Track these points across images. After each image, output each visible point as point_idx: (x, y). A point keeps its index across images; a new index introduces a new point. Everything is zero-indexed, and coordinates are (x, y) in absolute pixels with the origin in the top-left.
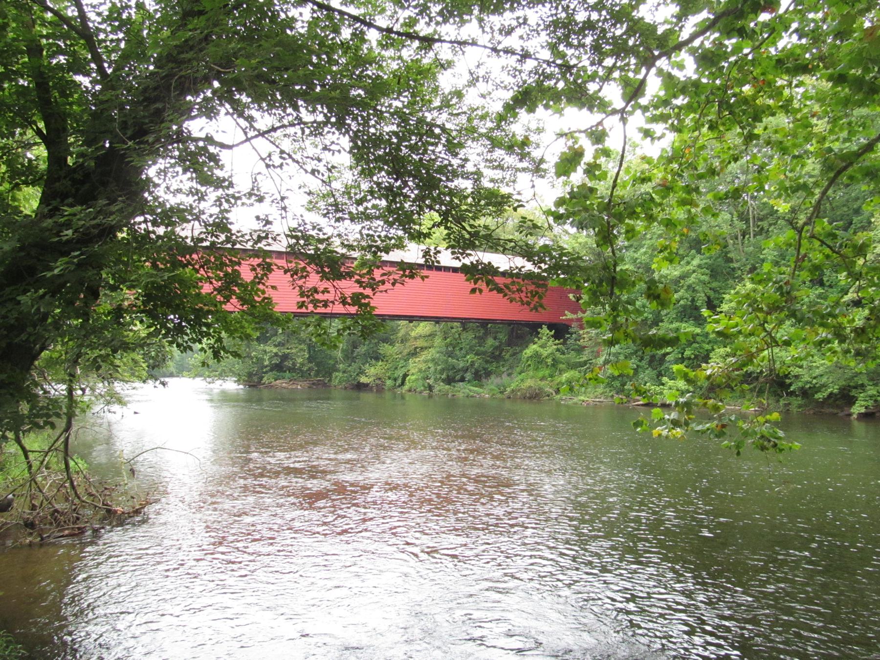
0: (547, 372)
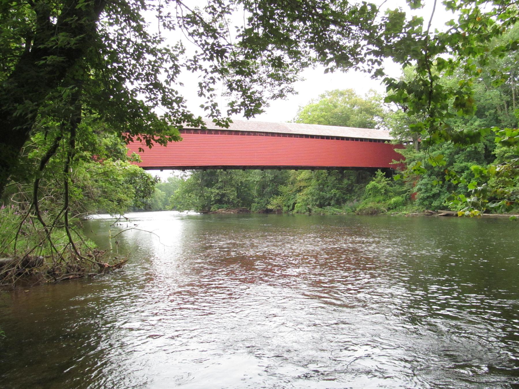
0: (382, 198)
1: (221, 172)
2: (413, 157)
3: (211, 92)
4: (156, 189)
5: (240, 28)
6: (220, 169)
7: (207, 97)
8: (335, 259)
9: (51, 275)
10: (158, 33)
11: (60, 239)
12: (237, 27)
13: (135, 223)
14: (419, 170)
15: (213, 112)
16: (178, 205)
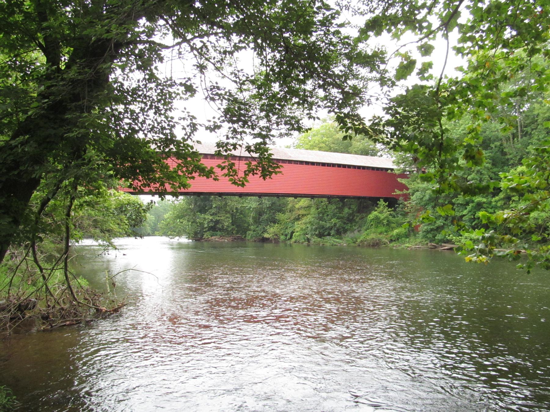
0: (384, 229)
14: (427, 219)
16: (170, 231)
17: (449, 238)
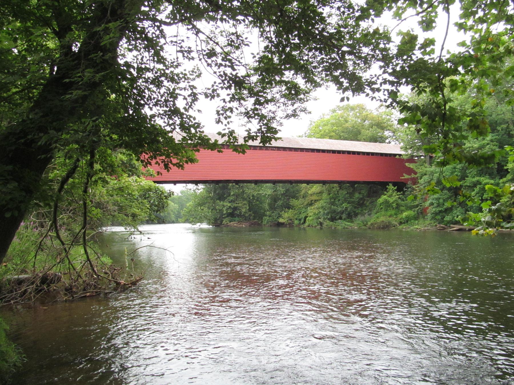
0: (393, 212)
1: (233, 186)
2: (424, 172)
3: (228, 120)
4: (169, 202)
5: (256, 55)
6: (232, 183)
7: (224, 124)
8: (347, 277)
9: (69, 293)
10: (176, 58)
11: (78, 254)
12: (253, 54)
13: (149, 236)
14: (433, 191)
15: (230, 139)
17: (457, 219)
